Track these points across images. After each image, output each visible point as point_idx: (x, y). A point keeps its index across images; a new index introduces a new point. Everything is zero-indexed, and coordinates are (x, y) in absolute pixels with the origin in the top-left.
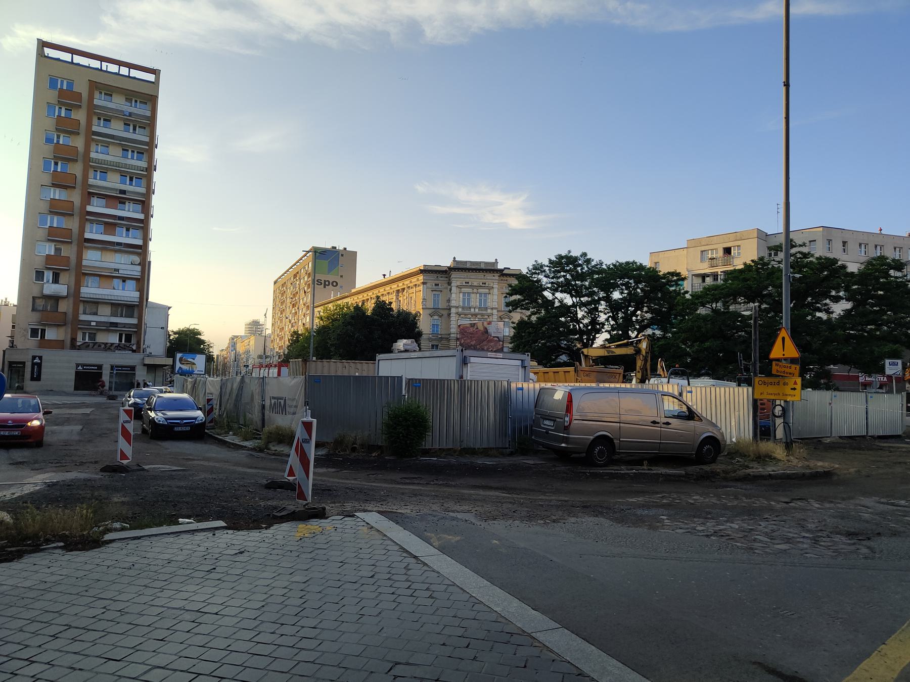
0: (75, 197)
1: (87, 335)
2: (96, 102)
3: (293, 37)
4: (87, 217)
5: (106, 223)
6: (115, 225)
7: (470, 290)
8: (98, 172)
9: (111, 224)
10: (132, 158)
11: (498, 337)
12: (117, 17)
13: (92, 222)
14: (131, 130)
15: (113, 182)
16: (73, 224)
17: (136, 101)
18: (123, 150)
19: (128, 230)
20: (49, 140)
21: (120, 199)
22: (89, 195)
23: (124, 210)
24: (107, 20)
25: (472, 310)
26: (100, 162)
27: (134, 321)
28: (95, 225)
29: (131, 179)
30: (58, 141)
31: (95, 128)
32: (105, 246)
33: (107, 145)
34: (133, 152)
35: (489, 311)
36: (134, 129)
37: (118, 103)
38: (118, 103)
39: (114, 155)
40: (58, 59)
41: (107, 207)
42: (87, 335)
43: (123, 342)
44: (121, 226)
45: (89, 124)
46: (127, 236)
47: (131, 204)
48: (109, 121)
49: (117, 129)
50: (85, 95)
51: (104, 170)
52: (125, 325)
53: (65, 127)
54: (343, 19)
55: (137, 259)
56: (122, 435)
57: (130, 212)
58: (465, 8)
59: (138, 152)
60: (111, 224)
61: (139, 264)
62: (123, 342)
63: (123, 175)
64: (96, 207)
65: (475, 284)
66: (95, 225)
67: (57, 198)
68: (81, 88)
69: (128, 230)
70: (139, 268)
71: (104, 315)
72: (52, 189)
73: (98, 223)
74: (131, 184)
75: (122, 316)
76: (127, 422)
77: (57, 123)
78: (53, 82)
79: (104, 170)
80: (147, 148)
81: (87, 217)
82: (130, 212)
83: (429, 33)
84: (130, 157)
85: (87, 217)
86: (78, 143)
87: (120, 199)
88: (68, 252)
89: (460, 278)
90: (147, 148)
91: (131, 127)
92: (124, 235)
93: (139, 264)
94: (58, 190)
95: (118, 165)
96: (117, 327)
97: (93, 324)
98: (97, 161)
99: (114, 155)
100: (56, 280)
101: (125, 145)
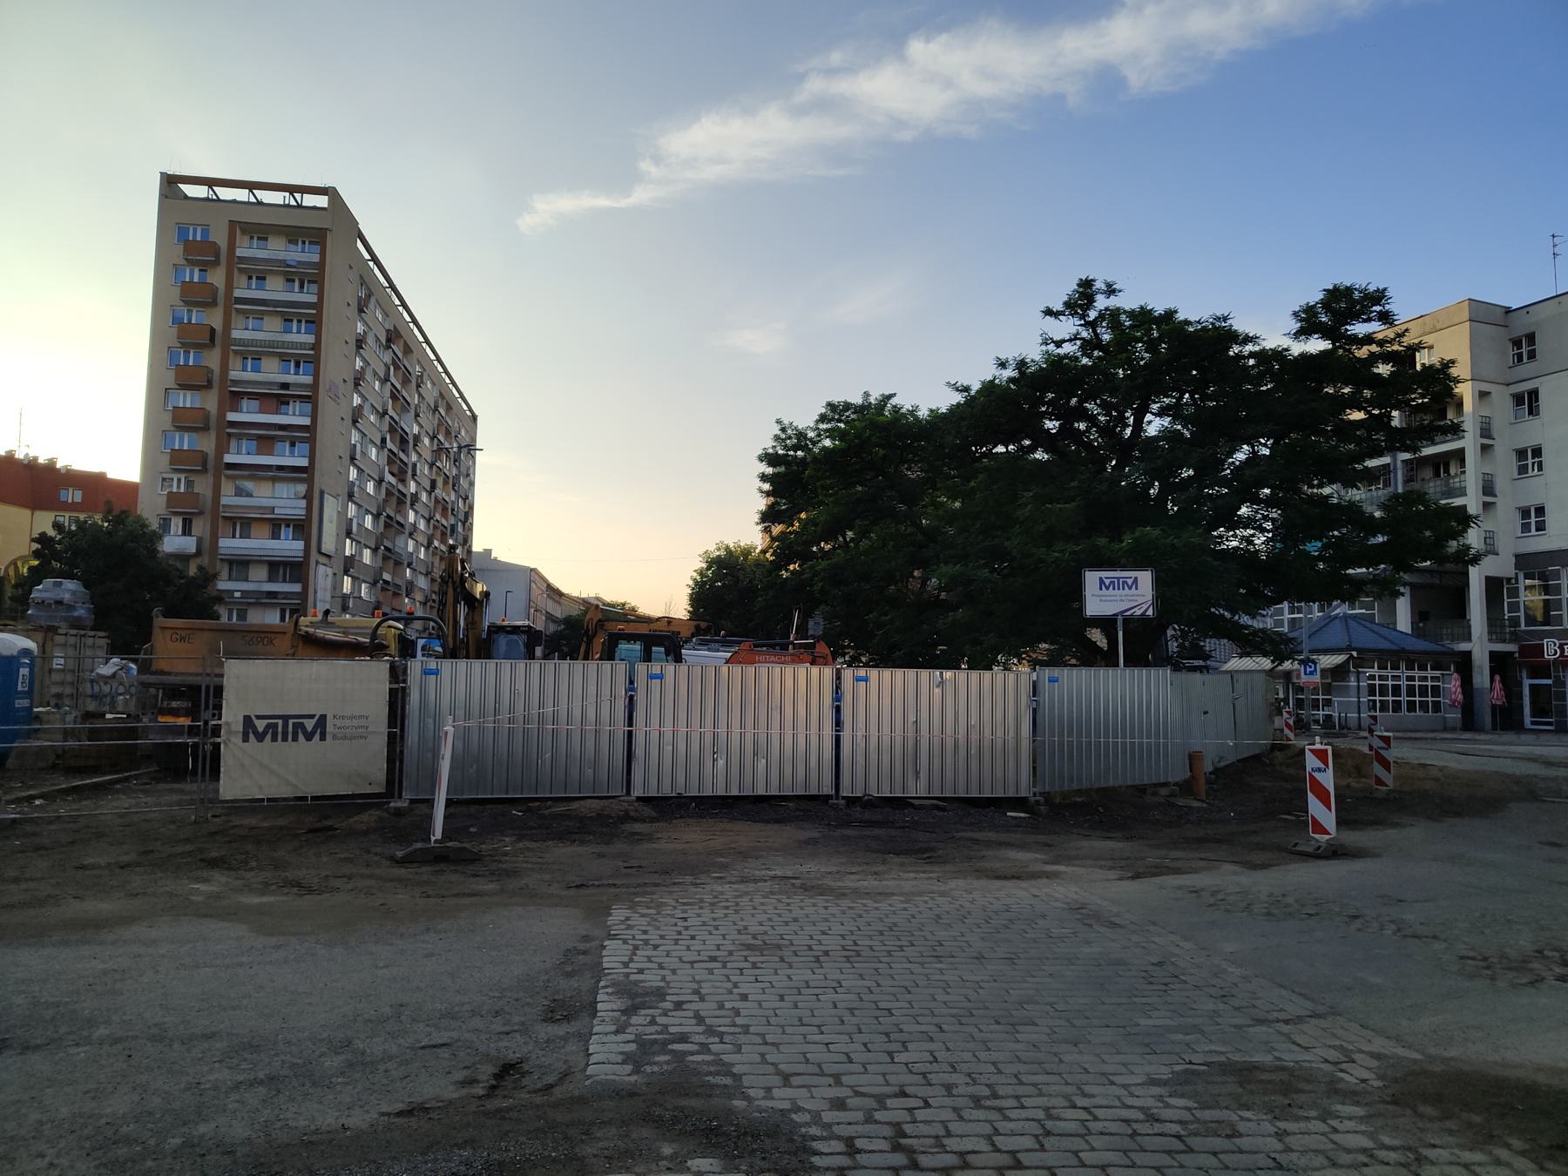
0: (210, 402)
1: (235, 612)
2: (239, 252)
3: (907, 136)
4: (230, 433)
5: (259, 437)
6: (272, 438)
8: (250, 360)
9: (266, 438)
10: (299, 332)
12: (657, 159)
13: (240, 437)
14: (297, 289)
15: (271, 372)
16: (207, 444)
17: (304, 242)
18: (285, 320)
19: (293, 445)
20: (177, 321)
21: (279, 398)
22: (234, 398)
23: (287, 414)
24: (645, 166)
26: (286, 345)
27: (297, 588)
28: (244, 441)
29: (297, 365)
30: (190, 320)
31: (238, 293)
32: (256, 472)
33: (260, 316)
34: (299, 321)
36: (302, 286)
37: (277, 249)
38: (277, 249)
39: (270, 330)
40: (234, 201)
41: (261, 411)
42: (235, 612)
43: (234, 620)
44: (282, 439)
45: (230, 286)
46: (292, 454)
47: (298, 403)
48: (264, 279)
49: (275, 289)
50: (223, 243)
51: (254, 354)
52: (287, 595)
53: (197, 296)
54: (985, 89)
55: (302, 488)
56: (1329, 793)
57: (294, 416)
58: (1200, 23)
59: (306, 322)
60: (266, 438)
61: (304, 498)
62: (234, 620)
63: (284, 358)
64: (247, 414)
66: (244, 441)
67: (188, 405)
68: (220, 237)
69: (293, 445)
70: (303, 503)
71: (258, 580)
72: (182, 392)
73: (250, 437)
74: (297, 373)
75: (284, 581)
76: (1319, 770)
77: (183, 294)
78: (182, 231)
79: (254, 354)
80: (314, 312)
81: (229, 430)
82: (294, 416)
83: (1135, 80)
84: (295, 330)
85: (230, 433)
86: (215, 319)
87: (279, 398)
88: (203, 486)
90: (314, 312)
91: (297, 284)
92: (287, 453)
93: (304, 498)
94: (189, 394)
95: (272, 344)
96: (276, 598)
97: (237, 595)
98: (240, 342)
99: (270, 330)
100: (187, 531)
101: (288, 313)
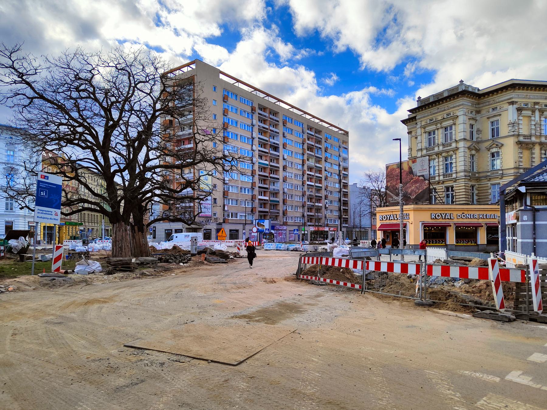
7: (433, 127)
11: (423, 176)
25: (436, 149)
35: (454, 145)
65: (440, 118)
89: (424, 117)
